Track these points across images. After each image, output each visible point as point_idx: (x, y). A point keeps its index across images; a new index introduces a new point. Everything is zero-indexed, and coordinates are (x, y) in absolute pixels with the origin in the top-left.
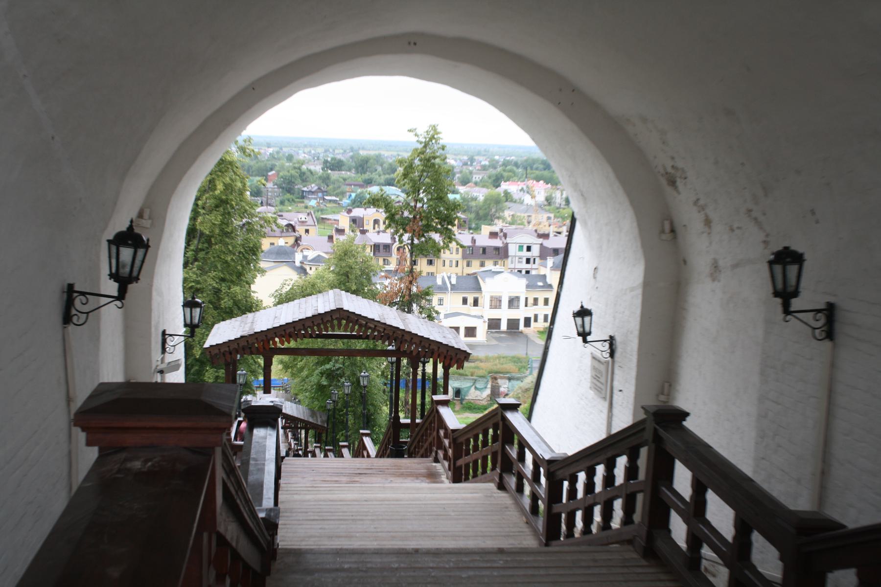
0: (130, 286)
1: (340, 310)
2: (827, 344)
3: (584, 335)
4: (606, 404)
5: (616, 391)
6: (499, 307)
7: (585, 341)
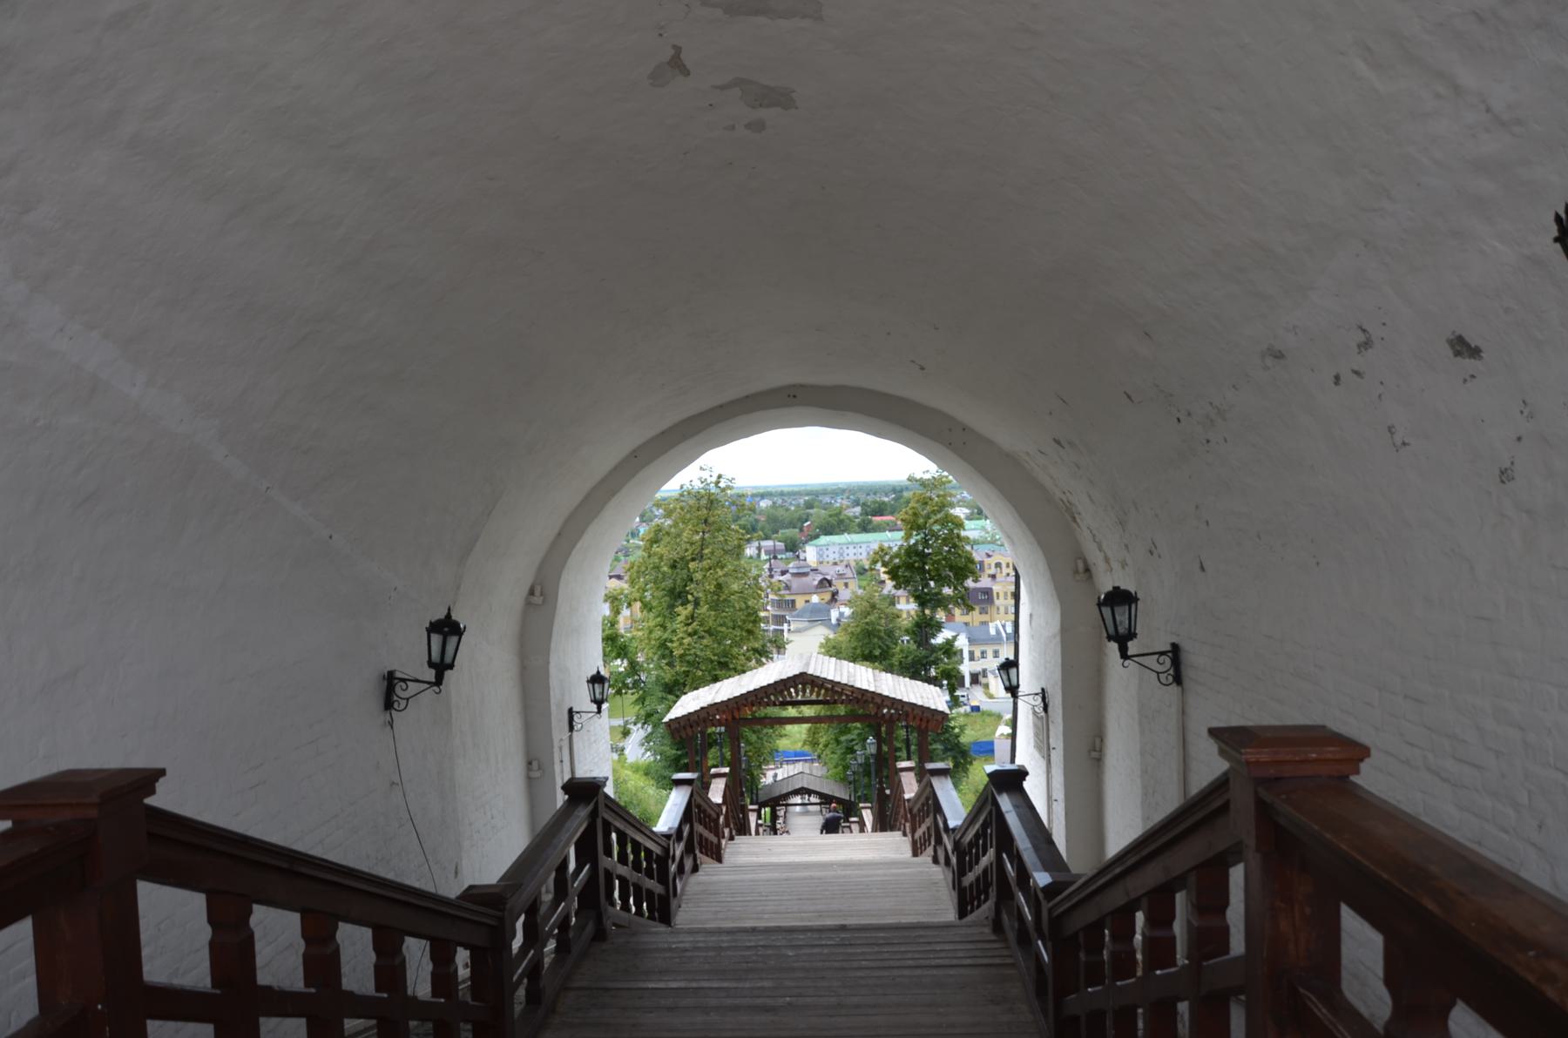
2: (1174, 688)
4: (1043, 763)
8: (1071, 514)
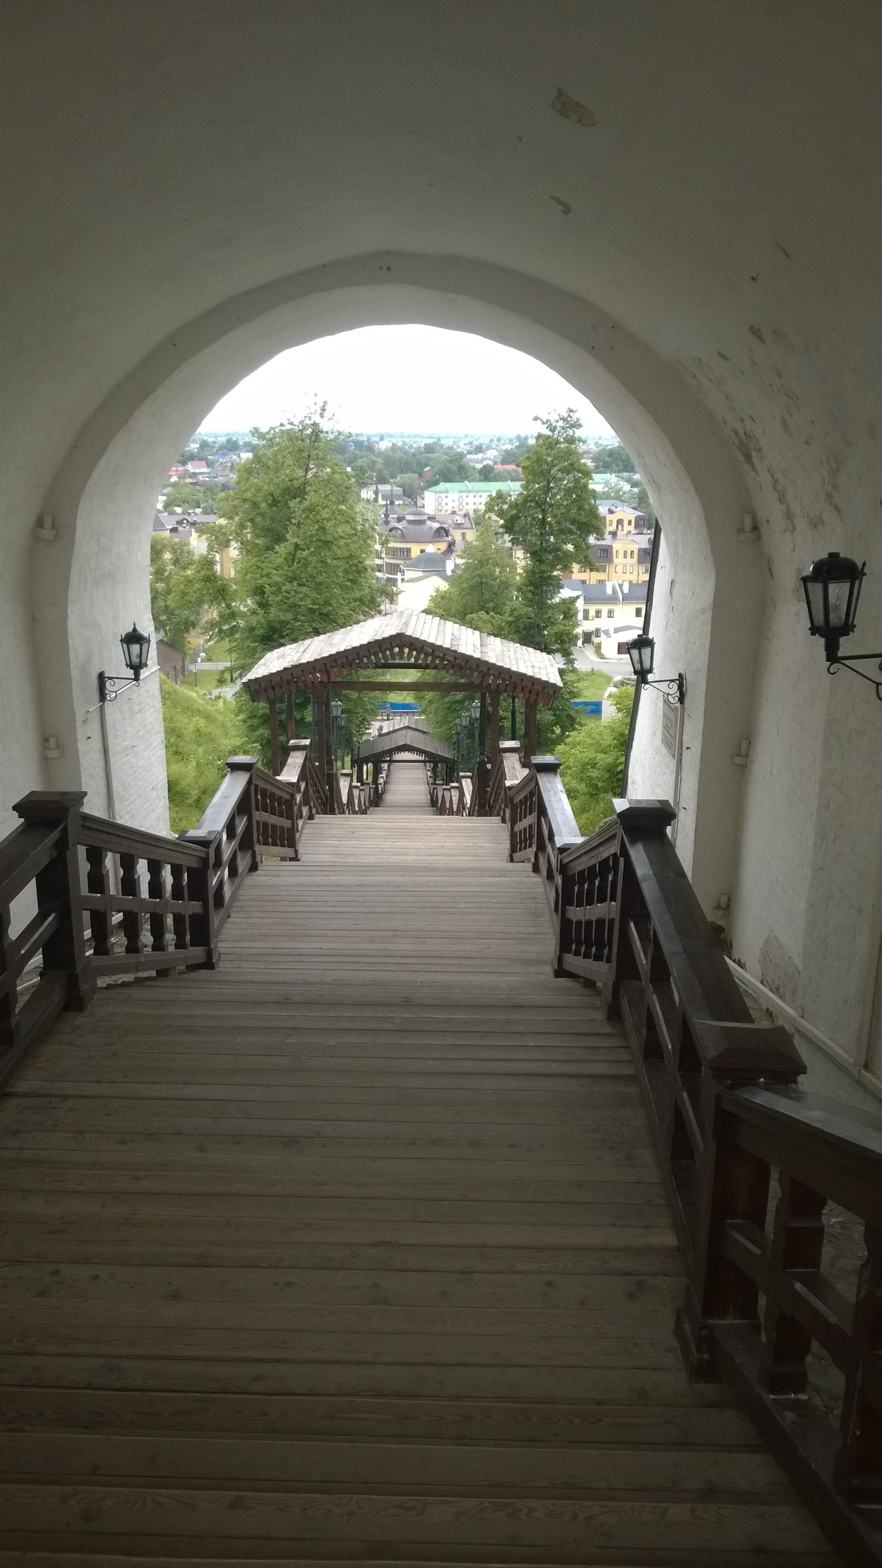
4: (673, 764)
8: (747, 450)
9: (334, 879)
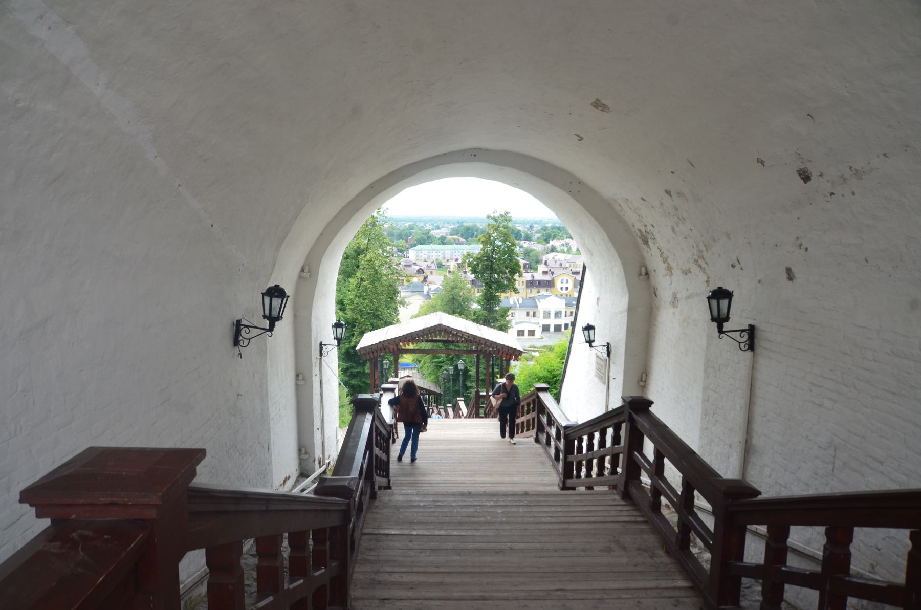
0: (277, 323)
1: (440, 325)
3: (590, 342)
5: (611, 379)
6: (549, 317)
7: (591, 346)
9: (435, 447)
